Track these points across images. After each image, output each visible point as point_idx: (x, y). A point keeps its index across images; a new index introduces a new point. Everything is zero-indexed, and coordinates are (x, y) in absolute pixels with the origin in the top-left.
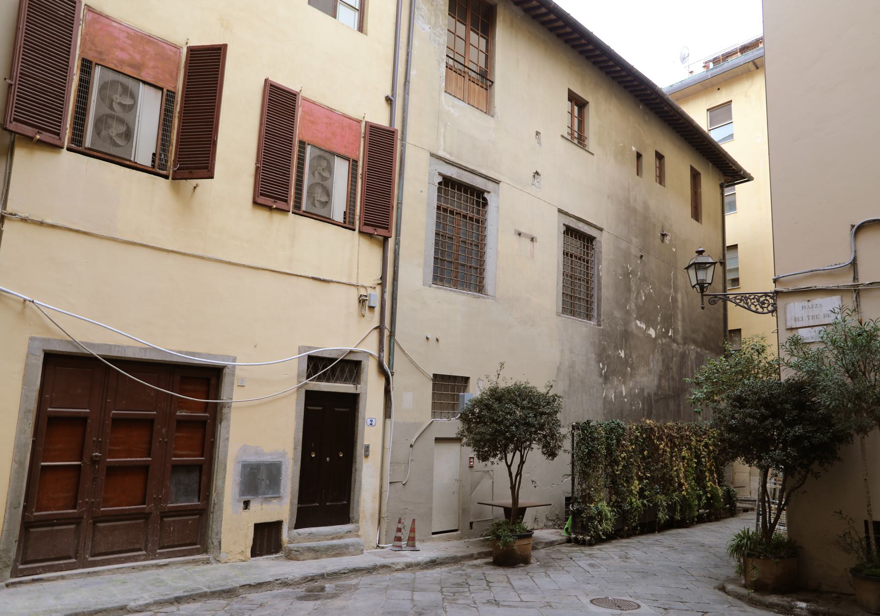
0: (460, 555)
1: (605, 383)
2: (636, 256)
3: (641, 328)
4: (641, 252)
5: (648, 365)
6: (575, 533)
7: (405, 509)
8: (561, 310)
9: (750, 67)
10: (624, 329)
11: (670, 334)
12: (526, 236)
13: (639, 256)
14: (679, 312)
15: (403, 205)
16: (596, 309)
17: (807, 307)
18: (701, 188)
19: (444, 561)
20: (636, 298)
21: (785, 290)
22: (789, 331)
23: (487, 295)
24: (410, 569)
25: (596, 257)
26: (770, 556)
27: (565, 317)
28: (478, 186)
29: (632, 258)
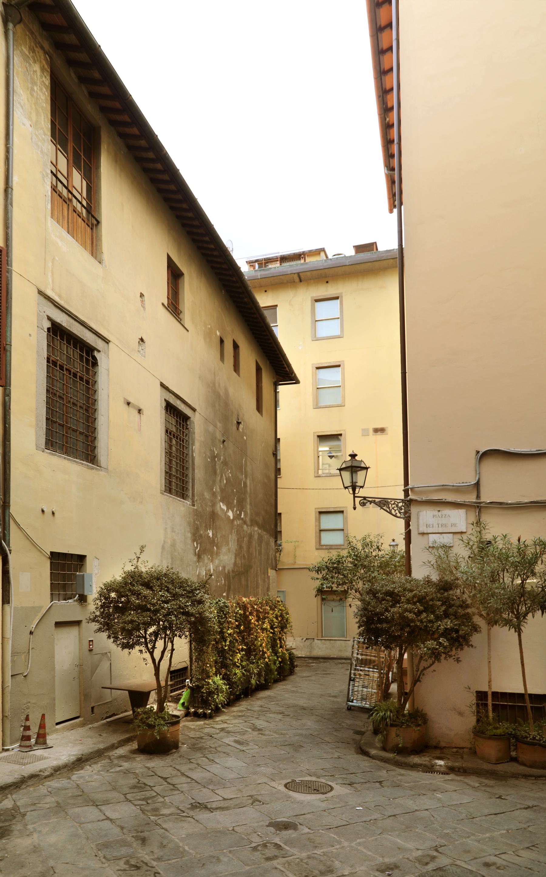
0: (102, 747)
1: (198, 561)
2: (219, 440)
3: (223, 510)
4: (223, 437)
5: (228, 545)
6: (194, 707)
7: (27, 703)
8: (164, 488)
9: (295, 278)
10: (211, 510)
11: (242, 517)
12: (134, 407)
13: (222, 440)
14: (248, 496)
15: (12, 347)
16: (191, 489)
17: (437, 516)
18: (262, 383)
19: (89, 756)
20: (220, 481)
21: (419, 499)
22: (420, 536)
23: (100, 467)
24: (58, 773)
25: (190, 438)
26: (412, 726)
27: (167, 496)
28: (88, 341)
29: (217, 441)
